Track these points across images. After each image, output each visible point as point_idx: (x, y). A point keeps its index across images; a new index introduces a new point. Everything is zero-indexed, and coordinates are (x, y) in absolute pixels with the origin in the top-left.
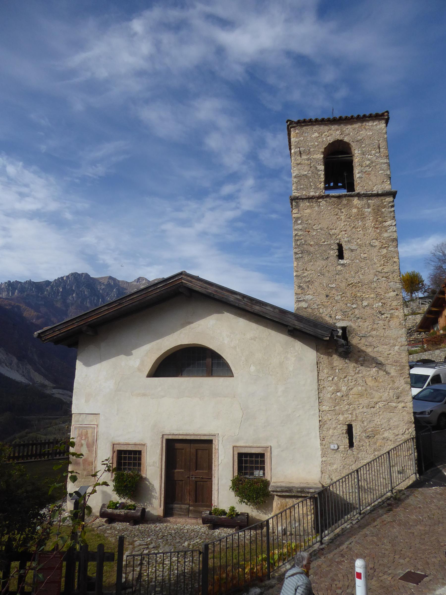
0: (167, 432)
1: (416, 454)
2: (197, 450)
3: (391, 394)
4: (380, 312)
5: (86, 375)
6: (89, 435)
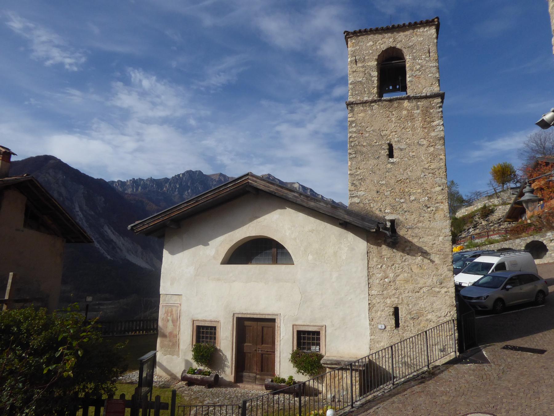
0: (237, 311)
1: (457, 334)
2: (263, 328)
3: (435, 280)
4: (426, 206)
6: (174, 312)
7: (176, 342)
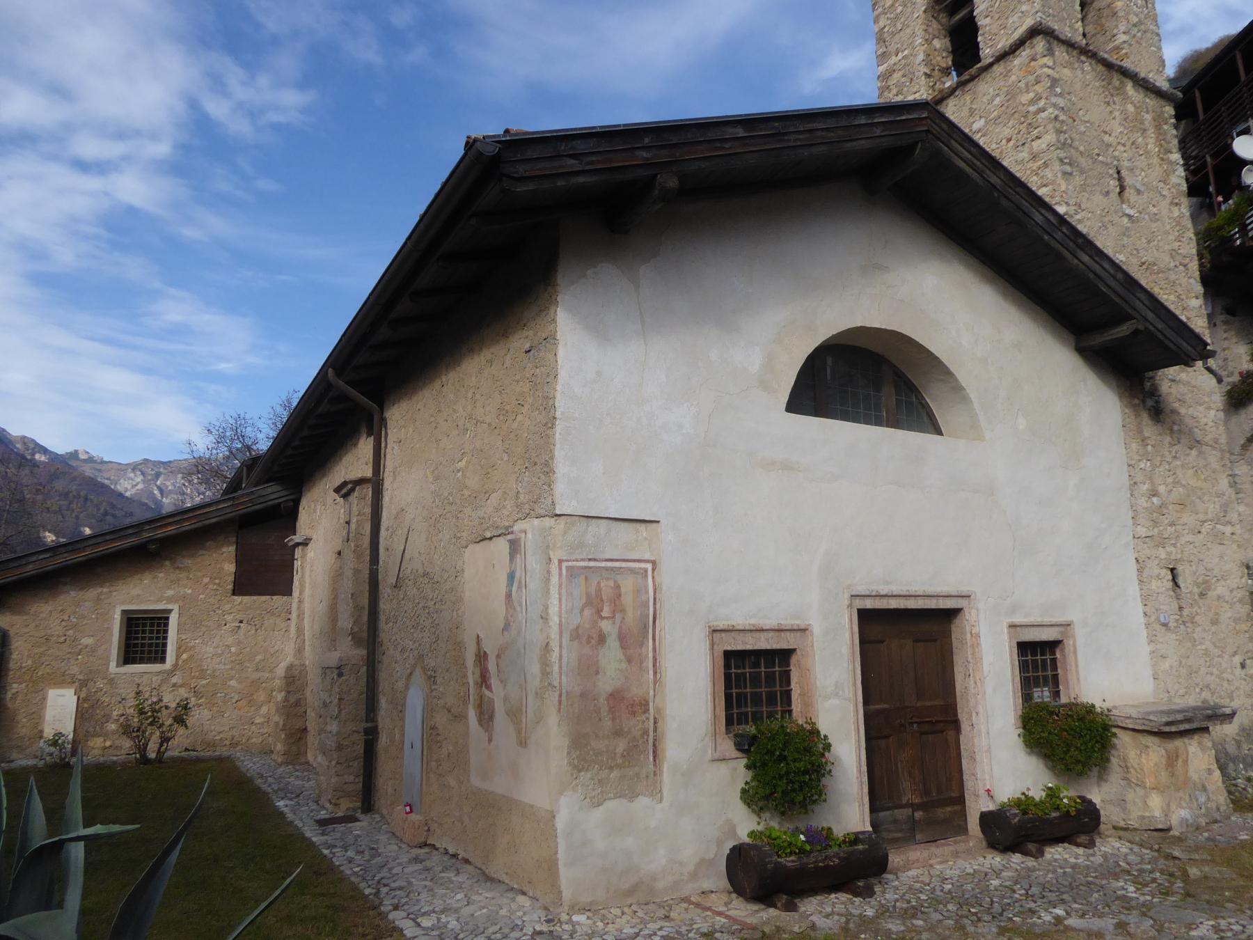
5: (599, 374)
6: (627, 599)
7: (645, 732)
